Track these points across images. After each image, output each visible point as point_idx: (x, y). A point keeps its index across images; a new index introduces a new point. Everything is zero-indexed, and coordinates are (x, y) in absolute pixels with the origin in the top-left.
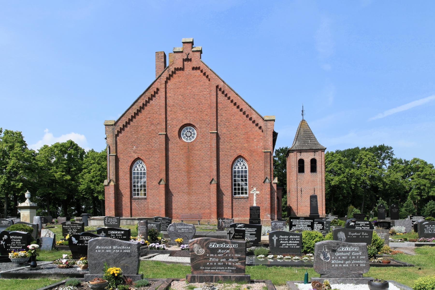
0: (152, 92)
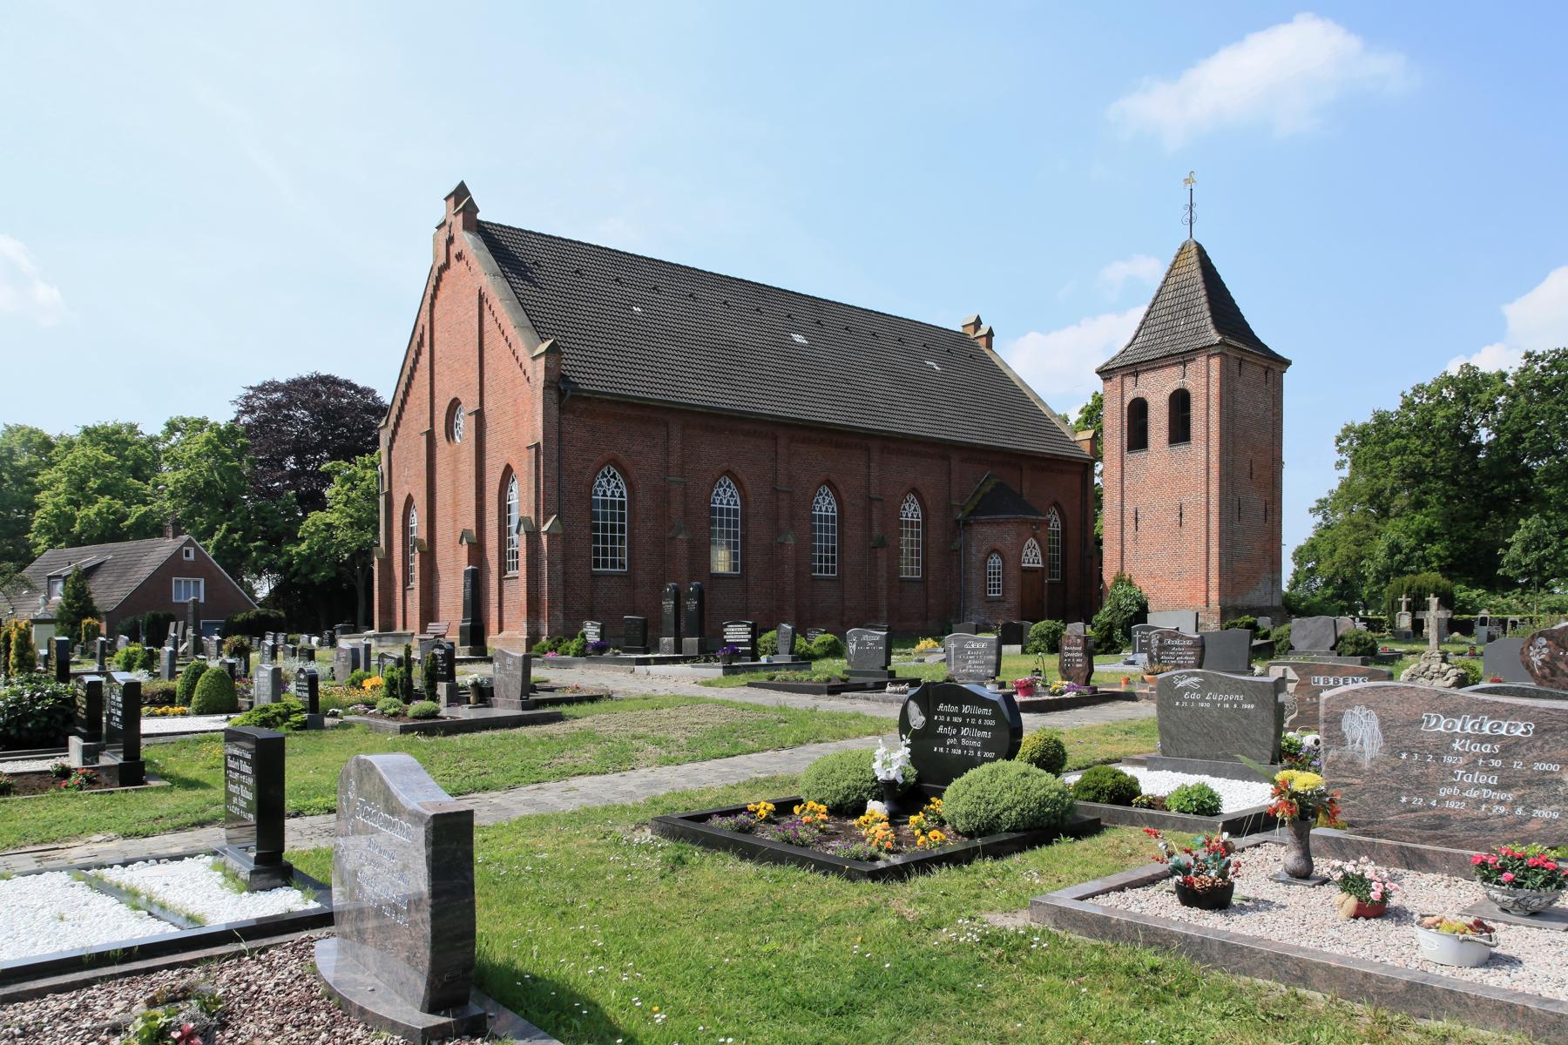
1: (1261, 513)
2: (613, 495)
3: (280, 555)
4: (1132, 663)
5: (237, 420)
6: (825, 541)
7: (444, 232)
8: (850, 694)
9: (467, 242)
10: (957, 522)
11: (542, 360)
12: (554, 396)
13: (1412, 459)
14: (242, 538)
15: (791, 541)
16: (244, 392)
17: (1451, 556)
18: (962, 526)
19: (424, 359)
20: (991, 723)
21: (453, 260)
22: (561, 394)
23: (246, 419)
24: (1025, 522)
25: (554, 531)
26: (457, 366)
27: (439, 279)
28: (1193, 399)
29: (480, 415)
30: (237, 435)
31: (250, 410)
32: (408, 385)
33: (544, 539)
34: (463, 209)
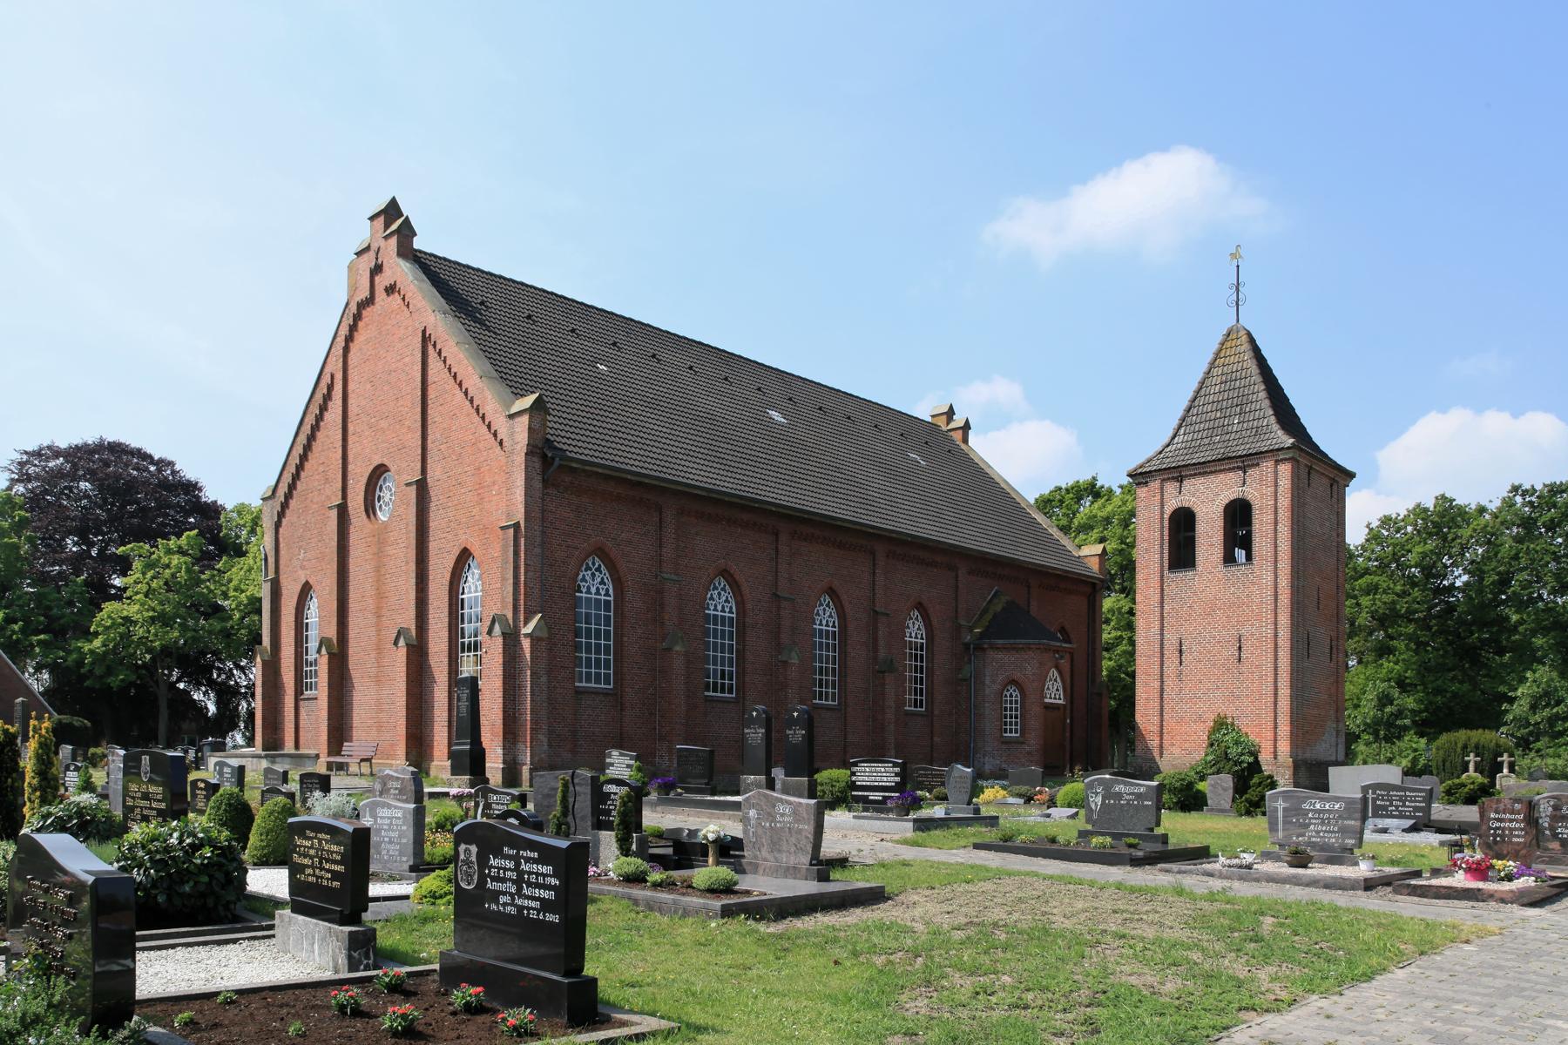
0: (323, 389)
1: (1327, 651)
2: (598, 593)
3: (69, 652)
4: (1384, 831)
5: (10, 488)
6: (826, 657)
7: (368, 261)
8: (1174, 867)
9: (401, 271)
10: (967, 646)
11: (525, 419)
12: (538, 465)
13: (1385, 598)
14: (22, 630)
15: (795, 660)
16: (17, 457)
17: (1426, 710)
18: (977, 648)
19: (334, 414)
20: (554, 881)
21: (380, 294)
22: (546, 462)
23: (20, 488)
24: (1048, 649)
25: (538, 634)
26: (384, 424)
27: (357, 317)
28: (1256, 513)
29: (422, 487)
30: (14, 506)
31: (25, 478)
32: (308, 448)
33: (526, 644)
34: (398, 231)
